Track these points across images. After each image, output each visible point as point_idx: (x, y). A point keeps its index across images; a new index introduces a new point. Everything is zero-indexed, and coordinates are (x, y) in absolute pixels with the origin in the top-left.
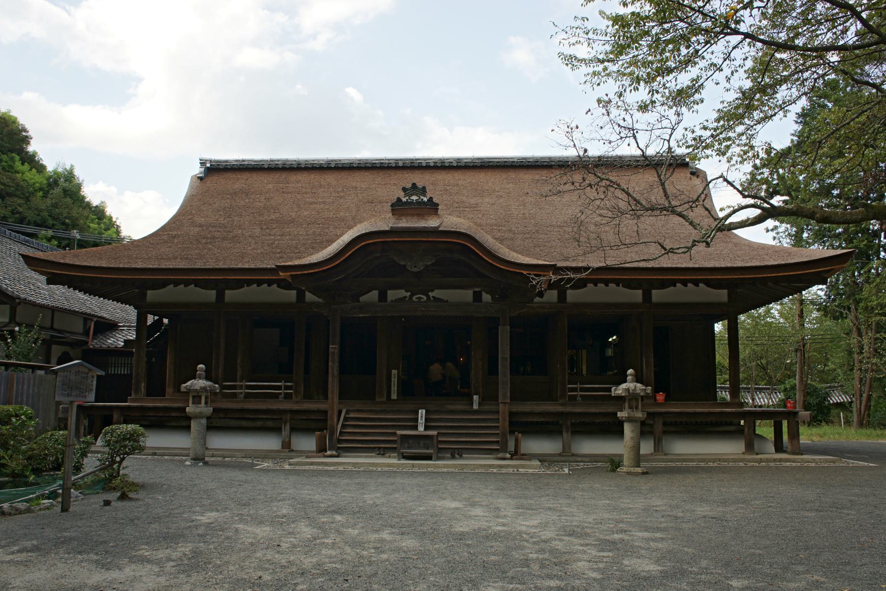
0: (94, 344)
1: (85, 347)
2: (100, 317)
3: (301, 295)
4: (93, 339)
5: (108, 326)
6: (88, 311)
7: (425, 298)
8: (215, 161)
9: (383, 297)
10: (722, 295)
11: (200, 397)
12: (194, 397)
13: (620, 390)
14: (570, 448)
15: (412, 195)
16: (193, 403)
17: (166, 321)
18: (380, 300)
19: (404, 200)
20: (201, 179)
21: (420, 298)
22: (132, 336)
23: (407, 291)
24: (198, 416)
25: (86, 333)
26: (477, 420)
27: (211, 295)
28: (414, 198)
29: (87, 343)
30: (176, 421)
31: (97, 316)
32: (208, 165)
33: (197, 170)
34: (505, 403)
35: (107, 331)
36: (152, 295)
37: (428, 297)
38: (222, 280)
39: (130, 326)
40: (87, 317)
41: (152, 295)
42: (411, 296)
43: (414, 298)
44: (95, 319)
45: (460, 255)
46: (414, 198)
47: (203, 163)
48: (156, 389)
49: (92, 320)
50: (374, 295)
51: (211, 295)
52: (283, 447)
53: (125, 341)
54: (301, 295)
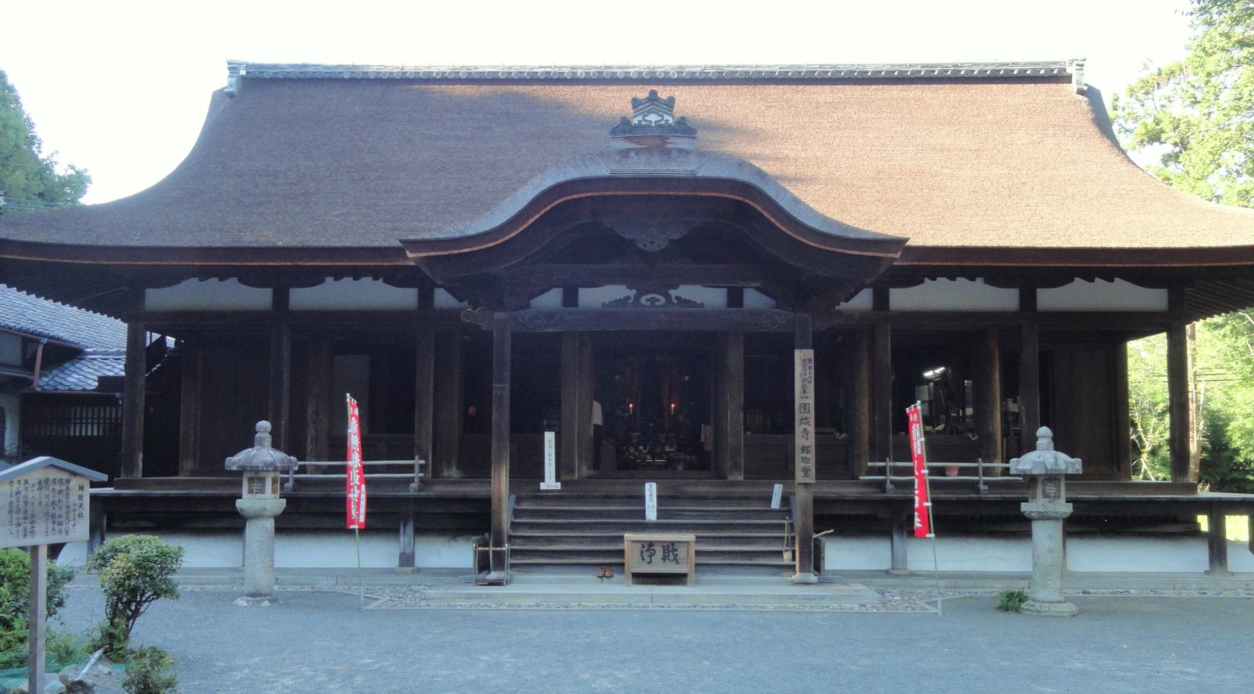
0: (44, 382)
1: (27, 391)
2: (52, 337)
3: (426, 297)
4: (41, 375)
5: (65, 354)
6: (32, 327)
7: (662, 300)
8: (253, 66)
9: (571, 298)
10: (1154, 299)
11: (262, 480)
12: (251, 480)
13: (1026, 463)
14: (905, 561)
15: (649, 112)
16: (251, 491)
17: (171, 341)
18: (565, 304)
19: (635, 121)
20: (231, 95)
21: (653, 300)
22: (118, 369)
23: (630, 288)
24: (1044, 517)
25: (28, 364)
26: (747, 514)
27: (261, 298)
28: (653, 118)
29: (31, 382)
30: (221, 519)
31: (45, 336)
32: (243, 73)
33: (223, 80)
34: (806, 485)
35: (66, 361)
36: (158, 299)
37: (668, 297)
38: (282, 269)
39: (106, 353)
40: (28, 340)
41: (158, 299)
42: (637, 298)
43: (643, 300)
44: (45, 340)
45: (736, 225)
46: (653, 118)
47: (233, 68)
48: (162, 461)
49: (38, 342)
50: (552, 299)
51: (261, 298)
52: (402, 564)
53: (102, 380)
54: (426, 297)
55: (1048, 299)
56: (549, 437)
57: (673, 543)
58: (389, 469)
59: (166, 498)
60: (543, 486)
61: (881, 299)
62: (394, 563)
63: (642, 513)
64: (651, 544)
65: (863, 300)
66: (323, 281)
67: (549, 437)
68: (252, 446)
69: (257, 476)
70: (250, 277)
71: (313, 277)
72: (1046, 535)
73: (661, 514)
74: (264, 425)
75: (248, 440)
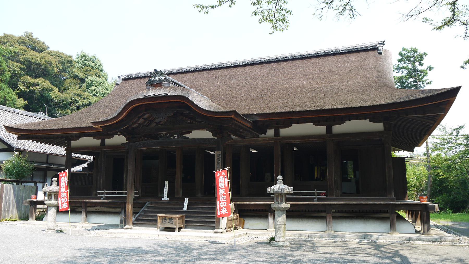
27: (322, 130)
51: (322, 130)
52: (121, 223)
55: (337, 129)
56: (166, 183)
57: (172, 217)
58: (118, 194)
59: (380, 205)
60: (163, 199)
61: (277, 133)
62: (118, 223)
63: (183, 208)
64: (165, 217)
65: (271, 132)
66: (291, 126)
67: (166, 183)
68: (276, 184)
69: (279, 196)
70: (317, 122)
71: (341, 121)
72: (281, 218)
73: (188, 209)
74: (280, 177)
75: (274, 182)
